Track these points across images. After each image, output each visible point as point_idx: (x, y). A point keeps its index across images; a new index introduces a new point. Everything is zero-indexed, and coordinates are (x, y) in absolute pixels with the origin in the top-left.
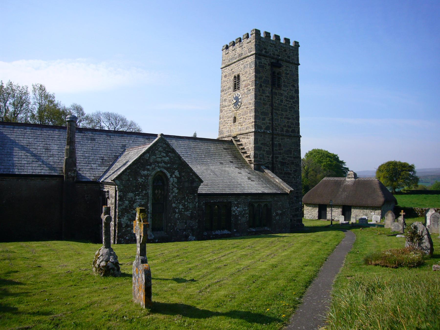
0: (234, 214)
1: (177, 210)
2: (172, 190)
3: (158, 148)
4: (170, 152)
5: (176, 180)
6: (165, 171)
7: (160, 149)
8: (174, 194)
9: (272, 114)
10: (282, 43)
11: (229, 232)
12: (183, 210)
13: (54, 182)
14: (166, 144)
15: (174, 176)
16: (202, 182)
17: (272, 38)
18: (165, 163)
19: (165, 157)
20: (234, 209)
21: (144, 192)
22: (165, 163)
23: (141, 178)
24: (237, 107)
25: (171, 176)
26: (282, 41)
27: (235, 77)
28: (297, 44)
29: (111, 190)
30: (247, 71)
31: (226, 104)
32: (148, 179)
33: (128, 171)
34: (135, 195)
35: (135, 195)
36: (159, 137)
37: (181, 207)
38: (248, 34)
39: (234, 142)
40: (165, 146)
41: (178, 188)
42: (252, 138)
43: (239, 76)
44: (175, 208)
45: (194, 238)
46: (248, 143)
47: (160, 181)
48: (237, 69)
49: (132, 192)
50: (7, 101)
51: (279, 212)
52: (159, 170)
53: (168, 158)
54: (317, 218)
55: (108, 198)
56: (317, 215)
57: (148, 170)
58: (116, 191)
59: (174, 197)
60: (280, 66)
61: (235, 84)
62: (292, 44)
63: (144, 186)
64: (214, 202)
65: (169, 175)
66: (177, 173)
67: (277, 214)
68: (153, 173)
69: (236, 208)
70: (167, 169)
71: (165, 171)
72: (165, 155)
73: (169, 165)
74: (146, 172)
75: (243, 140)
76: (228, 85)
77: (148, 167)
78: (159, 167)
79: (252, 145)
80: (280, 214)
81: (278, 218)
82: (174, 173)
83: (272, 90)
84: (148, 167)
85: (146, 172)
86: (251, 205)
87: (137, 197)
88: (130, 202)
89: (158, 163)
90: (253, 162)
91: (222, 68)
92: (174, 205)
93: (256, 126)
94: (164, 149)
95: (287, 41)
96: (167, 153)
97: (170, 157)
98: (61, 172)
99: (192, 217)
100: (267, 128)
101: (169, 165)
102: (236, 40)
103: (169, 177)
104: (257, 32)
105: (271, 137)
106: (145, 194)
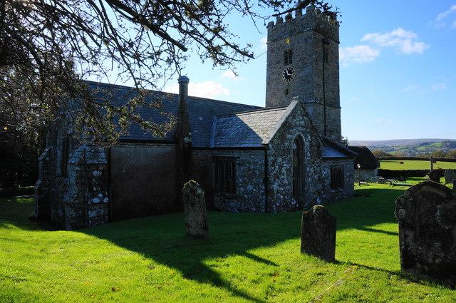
27: (291, 62)
94: (301, 112)
100: (321, 99)
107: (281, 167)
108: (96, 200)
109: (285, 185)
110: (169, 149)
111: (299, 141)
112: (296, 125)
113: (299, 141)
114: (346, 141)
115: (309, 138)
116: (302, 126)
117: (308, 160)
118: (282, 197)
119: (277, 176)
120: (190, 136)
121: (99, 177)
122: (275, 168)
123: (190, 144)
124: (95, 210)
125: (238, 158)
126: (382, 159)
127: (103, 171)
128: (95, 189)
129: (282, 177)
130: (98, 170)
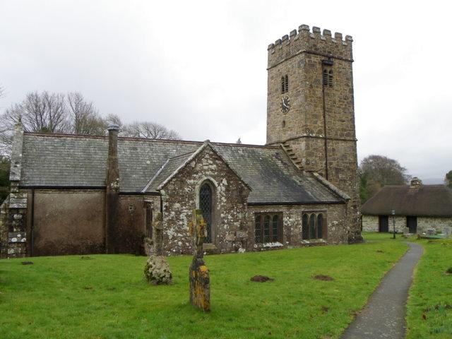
4: (217, 159)
7: (207, 156)
9: (324, 117)
27: (283, 78)
31: (274, 107)
43: (287, 77)
75: (293, 146)
76: (276, 87)
83: (323, 91)
94: (211, 156)
100: (320, 132)
105: (324, 141)
107: (179, 212)
108: (14, 240)
109: (186, 231)
110: (96, 195)
111: (207, 189)
112: (202, 170)
113: (207, 189)
114: (415, 181)
115: (225, 182)
116: (212, 170)
117: (222, 206)
118: (180, 243)
119: (171, 222)
120: (118, 182)
121: (20, 220)
122: (170, 213)
123: (117, 189)
124: (13, 248)
125: (153, 203)
126: (422, 216)
127: (23, 214)
128: (15, 230)
129: (181, 223)
130: (18, 213)
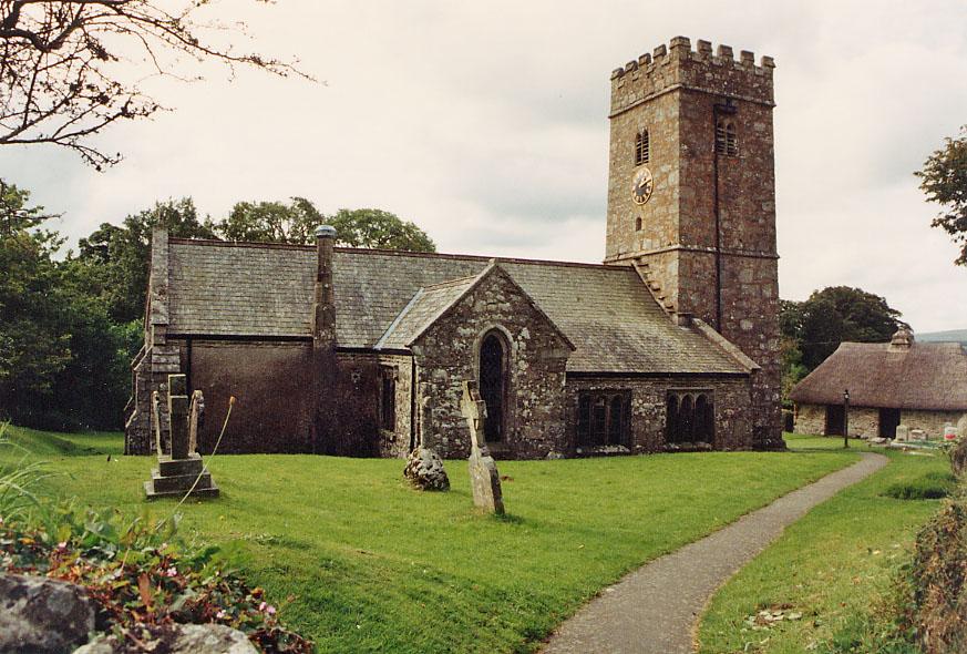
0: (636, 413)
1: (526, 403)
2: (517, 363)
3: (491, 287)
4: (513, 293)
5: (523, 344)
6: (504, 329)
8: (520, 372)
10: (738, 63)
11: (628, 450)
12: (538, 403)
13: (296, 351)
14: (505, 278)
15: (520, 338)
16: (710, 44)
17: (715, 54)
18: (503, 312)
19: (502, 302)
20: (635, 403)
21: (465, 367)
22: (503, 312)
23: (460, 342)
24: (643, 199)
25: (515, 338)
26: (737, 58)
27: (639, 136)
28: (769, 63)
29: (404, 366)
30: (666, 117)
32: (472, 343)
33: (436, 328)
34: (450, 373)
35: (450, 373)
36: (491, 265)
37: (533, 397)
38: (664, 46)
39: (637, 269)
40: (502, 281)
41: (526, 361)
42: (673, 266)
44: (523, 397)
45: (559, 456)
46: (666, 276)
47: (492, 347)
48: (639, 121)
49: (443, 367)
50: (259, 217)
51: (730, 412)
52: (492, 326)
53: (508, 304)
54: (823, 433)
55: (397, 379)
56: (823, 427)
57: (473, 326)
58: (414, 366)
59: (522, 377)
60: (732, 113)
61: (639, 151)
62: (758, 63)
63: (462, 357)
64: (597, 390)
65: (510, 336)
66: (525, 333)
67: (725, 417)
68: (482, 333)
69: (641, 401)
70: (507, 324)
71: (504, 329)
72: (503, 298)
73: (510, 317)
74: (468, 331)
77: (473, 321)
78: (492, 321)
79: (675, 282)
80: (732, 416)
81: (725, 424)
82: (520, 331)
84: (473, 321)
85: (468, 331)
86: (671, 400)
87: (453, 377)
88: (439, 384)
89: (490, 312)
90: (676, 308)
91: (611, 117)
92: (520, 393)
93: (682, 232)
95: (748, 55)
96: (507, 293)
97: (513, 303)
98: (307, 331)
99: (553, 417)
101: (510, 317)
102: (640, 58)
103: (511, 339)
104: (682, 43)
106: (467, 371)
